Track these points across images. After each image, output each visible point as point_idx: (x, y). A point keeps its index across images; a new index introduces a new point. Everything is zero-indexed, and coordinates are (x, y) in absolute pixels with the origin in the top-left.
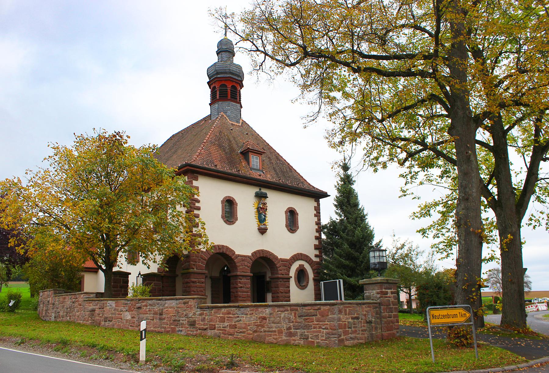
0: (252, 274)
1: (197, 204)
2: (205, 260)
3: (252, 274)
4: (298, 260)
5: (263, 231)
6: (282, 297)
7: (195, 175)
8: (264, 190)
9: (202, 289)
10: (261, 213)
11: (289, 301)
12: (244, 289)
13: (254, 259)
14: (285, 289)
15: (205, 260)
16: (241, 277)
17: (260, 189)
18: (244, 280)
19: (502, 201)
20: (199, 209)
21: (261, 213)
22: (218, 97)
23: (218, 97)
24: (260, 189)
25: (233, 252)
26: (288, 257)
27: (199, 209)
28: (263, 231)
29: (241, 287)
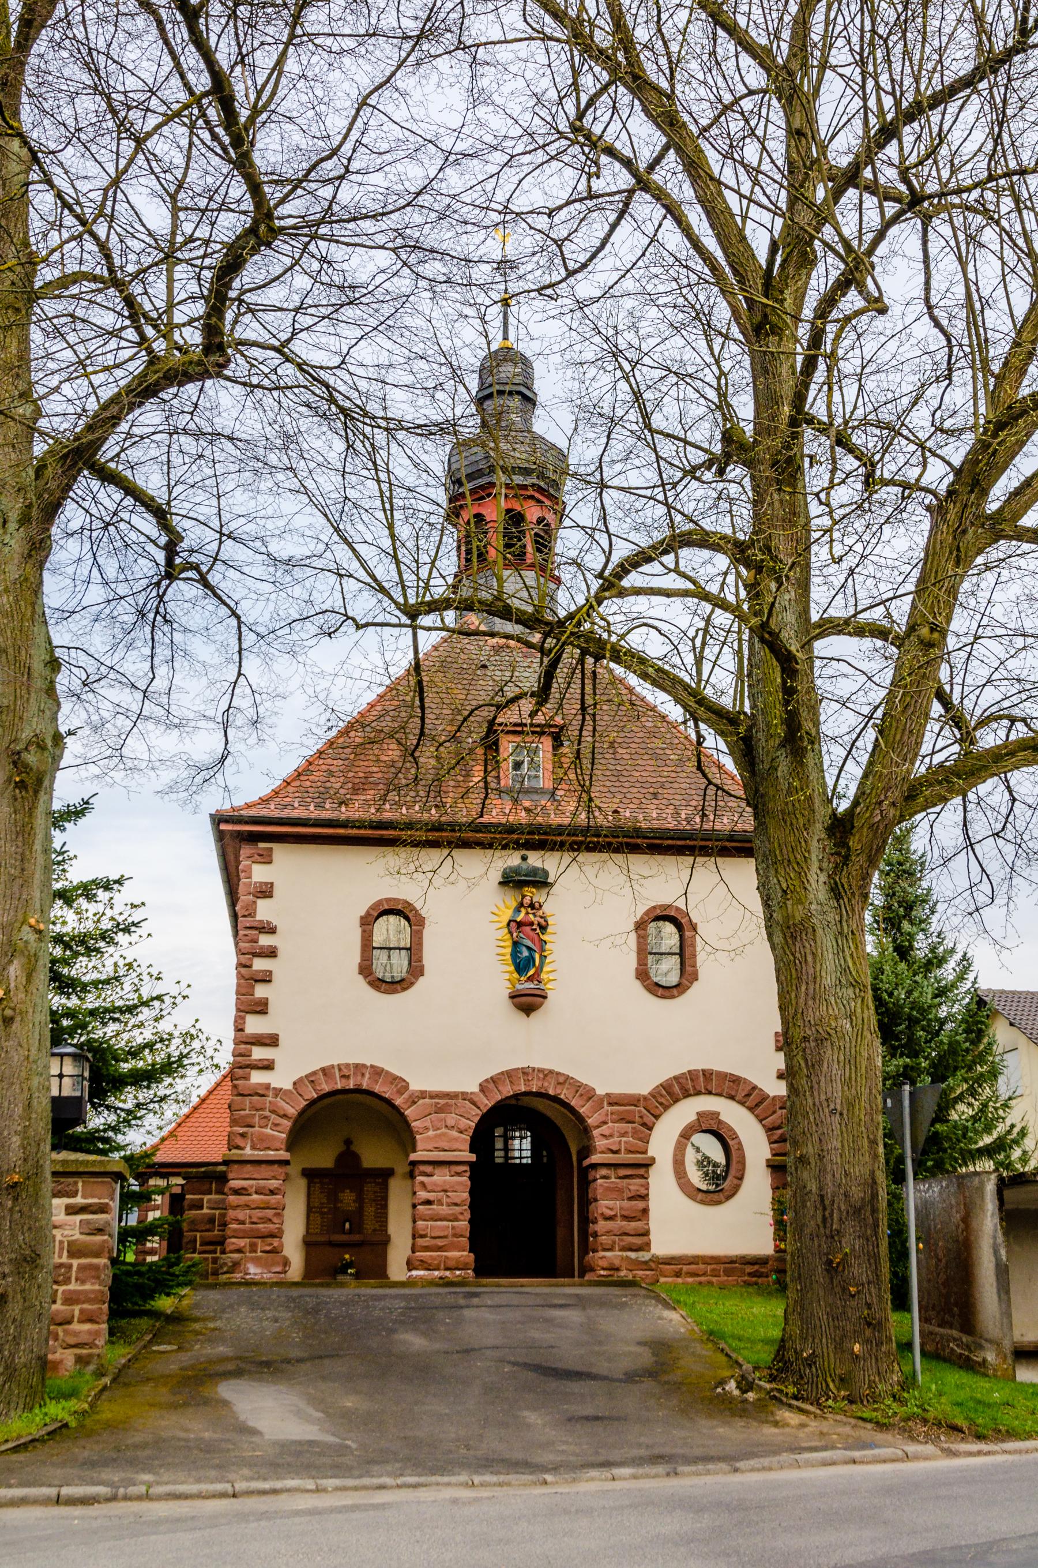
0: (473, 1157)
1: (265, 940)
2: (285, 1116)
3: (473, 1157)
4: (687, 1095)
5: (527, 1003)
6: (608, 1232)
7: (261, 845)
8: (536, 859)
9: (270, 1213)
10: (526, 950)
11: (646, 1246)
12: (444, 1210)
13: (487, 1103)
14: (626, 1204)
15: (285, 1116)
16: (428, 1169)
17: (524, 858)
18: (441, 1177)
19: (441, 496)
20: (271, 953)
21: (526, 950)
22: (223, 827)
23: (223, 827)
24: (524, 858)
25: (400, 1084)
26: (644, 1089)
27: (271, 953)
28: (527, 1003)
29: (428, 1202)
